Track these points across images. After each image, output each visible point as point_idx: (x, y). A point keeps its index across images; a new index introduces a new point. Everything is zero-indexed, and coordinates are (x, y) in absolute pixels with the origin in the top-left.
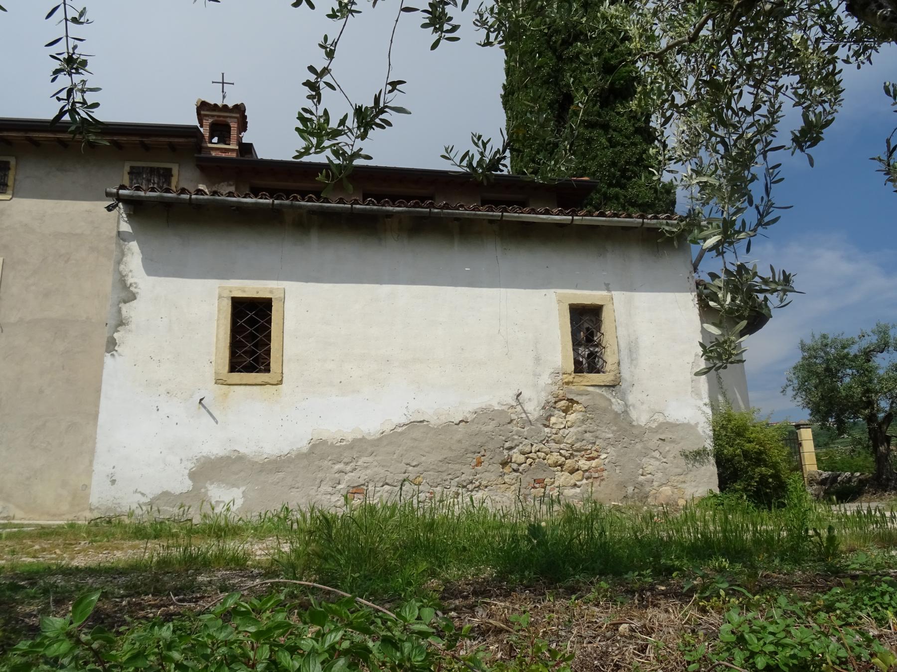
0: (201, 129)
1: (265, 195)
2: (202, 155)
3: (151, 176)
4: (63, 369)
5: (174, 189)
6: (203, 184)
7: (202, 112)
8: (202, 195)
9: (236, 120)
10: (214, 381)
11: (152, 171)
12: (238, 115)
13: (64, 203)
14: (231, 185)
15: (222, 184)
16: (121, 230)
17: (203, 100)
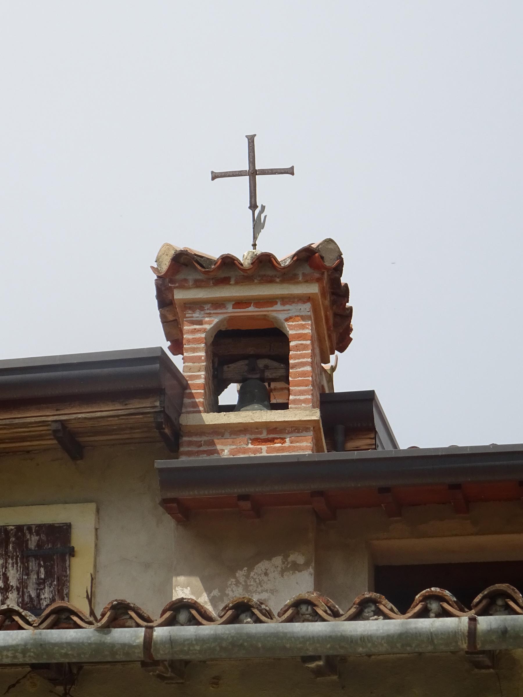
0: (177, 361)
1: (440, 599)
2: (183, 461)
5: (82, 606)
6: (190, 573)
7: (179, 295)
8: (192, 621)
9: (306, 308)
12: (314, 289)
14: (296, 567)
17: (180, 246)
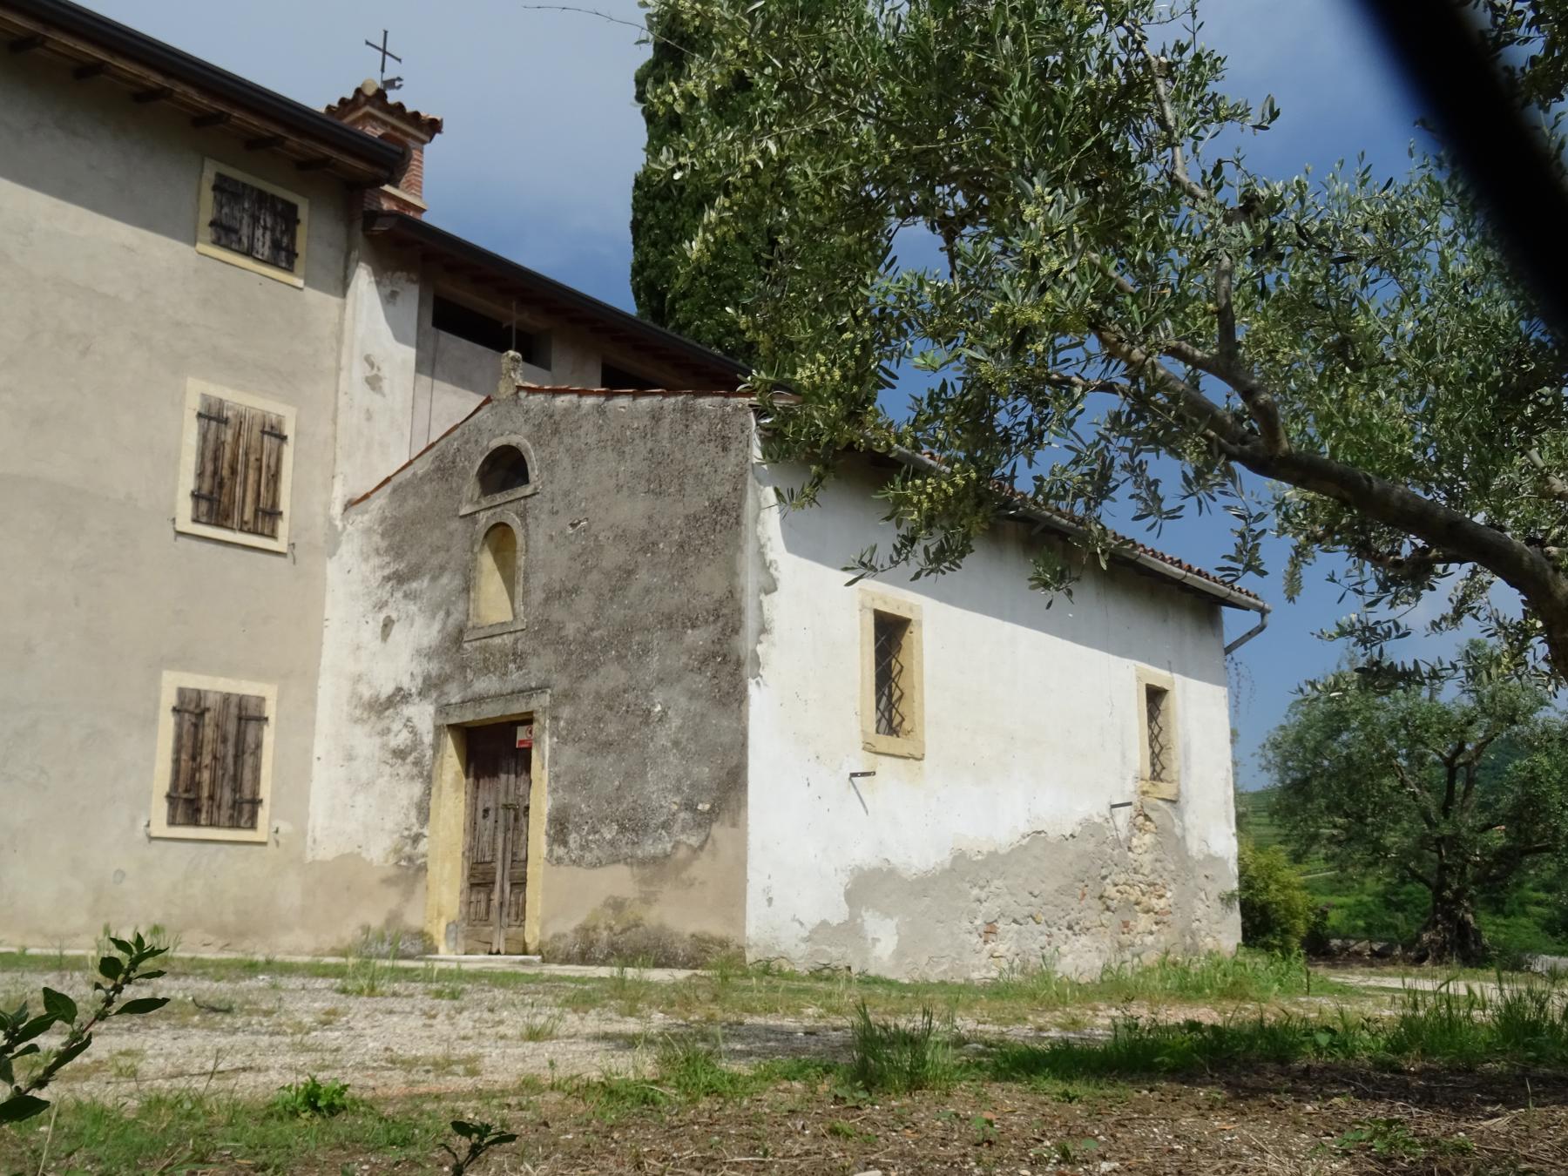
3: (260, 209)
4: (77, 605)
10: (861, 745)
11: (263, 199)
13: (73, 212)
15: (398, 274)
16: (1227, 612)
